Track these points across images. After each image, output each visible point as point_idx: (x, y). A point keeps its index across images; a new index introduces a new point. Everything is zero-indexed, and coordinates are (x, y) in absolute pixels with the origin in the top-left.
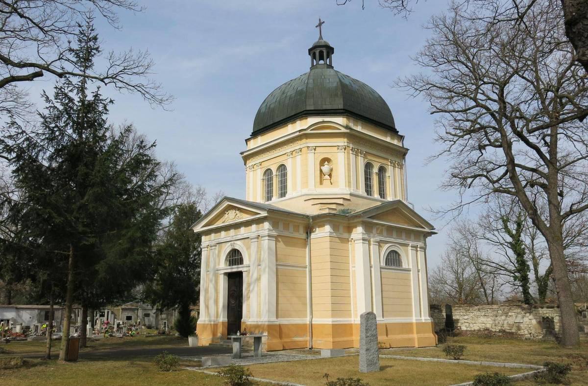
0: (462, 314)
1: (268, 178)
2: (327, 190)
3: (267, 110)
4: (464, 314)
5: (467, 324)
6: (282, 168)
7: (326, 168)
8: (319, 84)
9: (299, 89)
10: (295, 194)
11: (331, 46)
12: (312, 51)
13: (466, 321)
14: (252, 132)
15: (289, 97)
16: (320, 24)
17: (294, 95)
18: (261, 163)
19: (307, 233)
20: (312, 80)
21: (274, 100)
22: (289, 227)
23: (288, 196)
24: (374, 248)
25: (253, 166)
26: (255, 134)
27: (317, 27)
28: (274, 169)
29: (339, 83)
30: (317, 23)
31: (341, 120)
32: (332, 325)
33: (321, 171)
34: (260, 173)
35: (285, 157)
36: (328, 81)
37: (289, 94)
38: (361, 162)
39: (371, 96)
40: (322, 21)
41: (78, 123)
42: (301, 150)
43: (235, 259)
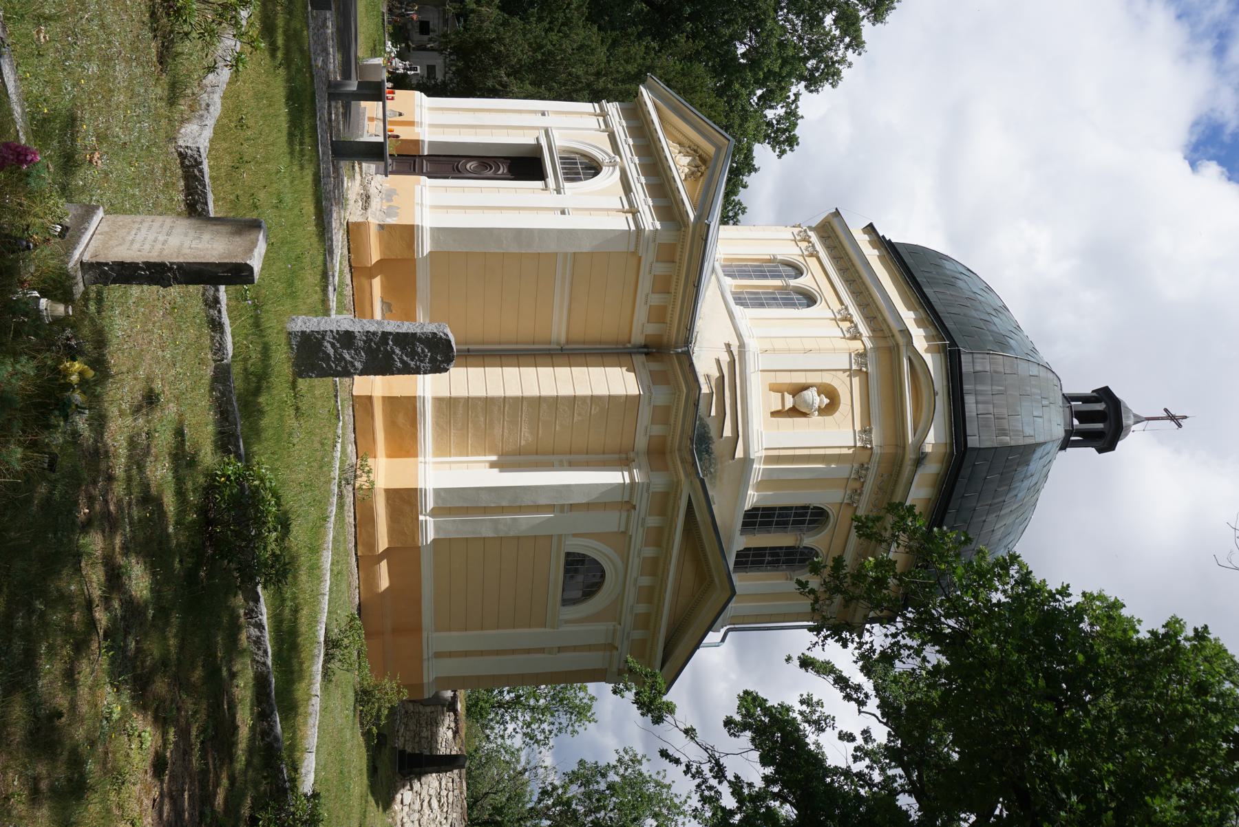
0: (444, 793)
3: (948, 272)
4: (444, 800)
5: (417, 806)
6: (810, 299)
7: (818, 400)
8: (1028, 389)
11: (1120, 444)
12: (1105, 394)
13: (425, 804)
14: (893, 241)
15: (988, 319)
16: (1172, 418)
17: (996, 330)
18: (814, 254)
19: (645, 346)
22: (662, 262)
23: (738, 310)
24: (611, 521)
27: (1166, 410)
28: (804, 282)
29: (1031, 441)
30: (1175, 412)
31: (934, 439)
32: (422, 685)
33: (805, 387)
34: (791, 251)
35: (836, 306)
37: (996, 320)
38: (828, 498)
39: (998, 535)
40: (1183, 422)
42: (856, 336)
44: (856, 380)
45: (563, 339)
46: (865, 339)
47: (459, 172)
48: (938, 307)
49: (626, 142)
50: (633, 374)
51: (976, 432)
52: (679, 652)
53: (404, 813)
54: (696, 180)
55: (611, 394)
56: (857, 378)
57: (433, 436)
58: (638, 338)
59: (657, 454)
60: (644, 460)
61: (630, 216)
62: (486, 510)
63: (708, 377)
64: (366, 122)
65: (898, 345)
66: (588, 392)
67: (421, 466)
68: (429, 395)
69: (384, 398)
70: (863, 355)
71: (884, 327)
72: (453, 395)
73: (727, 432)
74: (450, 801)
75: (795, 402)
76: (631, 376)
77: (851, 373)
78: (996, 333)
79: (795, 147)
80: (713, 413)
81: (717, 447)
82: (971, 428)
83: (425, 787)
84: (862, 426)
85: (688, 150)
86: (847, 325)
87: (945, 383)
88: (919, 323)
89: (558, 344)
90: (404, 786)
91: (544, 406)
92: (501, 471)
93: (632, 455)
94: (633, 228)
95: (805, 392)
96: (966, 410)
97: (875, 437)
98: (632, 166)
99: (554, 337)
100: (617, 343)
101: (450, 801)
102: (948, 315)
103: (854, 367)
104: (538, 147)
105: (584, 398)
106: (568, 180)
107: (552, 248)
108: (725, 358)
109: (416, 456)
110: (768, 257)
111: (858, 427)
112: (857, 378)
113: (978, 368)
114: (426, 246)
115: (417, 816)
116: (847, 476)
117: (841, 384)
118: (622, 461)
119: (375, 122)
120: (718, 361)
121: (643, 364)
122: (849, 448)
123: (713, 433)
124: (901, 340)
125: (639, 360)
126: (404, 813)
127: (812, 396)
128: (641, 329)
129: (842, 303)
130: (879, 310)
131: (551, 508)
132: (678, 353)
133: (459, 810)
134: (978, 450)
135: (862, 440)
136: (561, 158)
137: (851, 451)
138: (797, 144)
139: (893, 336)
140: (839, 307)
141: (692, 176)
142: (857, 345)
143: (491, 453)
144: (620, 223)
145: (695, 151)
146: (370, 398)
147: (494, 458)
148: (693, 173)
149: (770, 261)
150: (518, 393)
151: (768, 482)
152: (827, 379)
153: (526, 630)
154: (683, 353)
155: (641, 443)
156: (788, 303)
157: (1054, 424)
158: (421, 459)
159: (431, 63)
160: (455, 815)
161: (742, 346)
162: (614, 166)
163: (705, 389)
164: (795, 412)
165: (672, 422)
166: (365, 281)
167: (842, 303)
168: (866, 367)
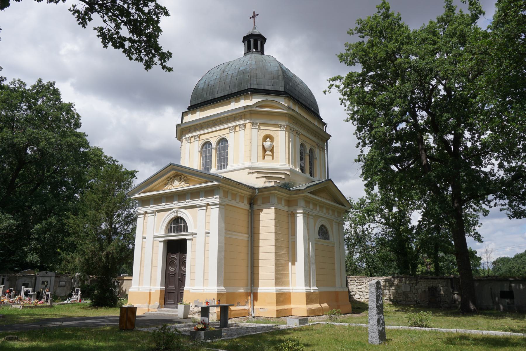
0: (356, 284)
1: (206, 151)
2: (268, 164)
4: (359, 284)
5: (361, 293)
6: (223, 141)
7: (267, 144)
9: (241, 69)
10: (236, 167)
13: (360, 290)
15: (230, 76)
16: (254, 16)
18: (199, 136)
19: (250, 204)
20: (254, 62)
21: (214, 77)
22: (228, 196)
24: (311, 221)
25: (190, 138)
26: (193, 108)
27: (251, 18)
33: (263, 146)
34: (197, 145)
35: (227, 131)
36: (269, 65)
41: (490, 80)
42: (244, 125)
43: (178, 226)
44: (262, 128)
45: (247, 236)
46: (245, 122)
47: (175, 274)
48: (226, 93)
49: (164, 205)
50: (263, 210)
51: (278, 87)
52: (342, 200)
53: (363, 298)
54: (188, 179)
55: (274, 218)
56: (261, 127)
57: (285, 286)
58: (247, 207)
59: (291, 203)
60: (292, 209)
61: (209, 207)
62: (309, 267)
63: (265, 182)
64: (150, 312)
65: (250, 111)
66: (274, 227)
67: (294, 291)
68: (274, 288)
69: (277, 305)
70: (253, 124)
71: (240, 114)
72: (274, 279)
73: (283, 177)
74: (359, 281)
75: (268, 151)
76: (264, 211)
77: (259, 129)
78: (238, 73)
79: (86, 134)
80: (279, 181)
81: (287, 181)
82: (277, 89)
83: (354, 290)
84: (278, 127)
85: (170, 181)
86: (237, 128)
87: (264, 96)
88: (237, 101)
89: (249, 237)
90: (353, 298)
91: (277, 244)
92: (297, 261)
93: (290, 212)
94: (218, 206)
95: (265, 147)
96: (272, 89)
97: (283, 123)
98: (179, 204)
99: (246, 239)
100: (248, 215)
101: (359, 281)
102: (230, 90)
103: (257, 127)
104: (164, 241)
105: (276, 229)
106: (187, 231)
107: (223, 238)
108: (256, 175)
109: (290, 293)
110: (200, 154)
111: (279, 129)
112: (261, 127)
113: (256, 83)
114: (314, 288)
115: (364, 293)
116: (293, 135)
117: (263, 133)
118: (293, 216)
119: (150, 308)
120: (257, 178)
121: (258, 206)
122: (286, 133)
123: (283, 182)
124: (249, 109)
125: (256, 207)
126: (363, 298)
127: (267, 144)
128: (245, 206)
129: (227, 128)
130: (232, 115)
131: (309, 243)
132: (258, 193)
133: (362, 278)
134: (285, 88)
135: (283, 128)
136: (168, 233)
137: (287, 133)
138: (85, 133)
139: (245, 112)
140: (228, 130)
141: (187, 181)
142: (248, 126)
143: (288, 265)
144: (215, 212)
145: (171, 178)
146: (277, 311)
147: (290, 264)
148: (185, 181)
149: (201, 153)
150: (274, 254)
151: (294, 164)
152: (261, 138)
153: (335, 254)
154: (258, 191)
155: (286, 208)
156: (226, 148)
157: (254, 56)
158: (291, 291)
159: (41, 283)
160: (364, 280)
161: (249, 168)
162: (178, 211)
163: (272, 184)
164: (272, 150)
165: (281, 197)
166: (233, 313)
167: (227, 128)
168: (257, 123)
